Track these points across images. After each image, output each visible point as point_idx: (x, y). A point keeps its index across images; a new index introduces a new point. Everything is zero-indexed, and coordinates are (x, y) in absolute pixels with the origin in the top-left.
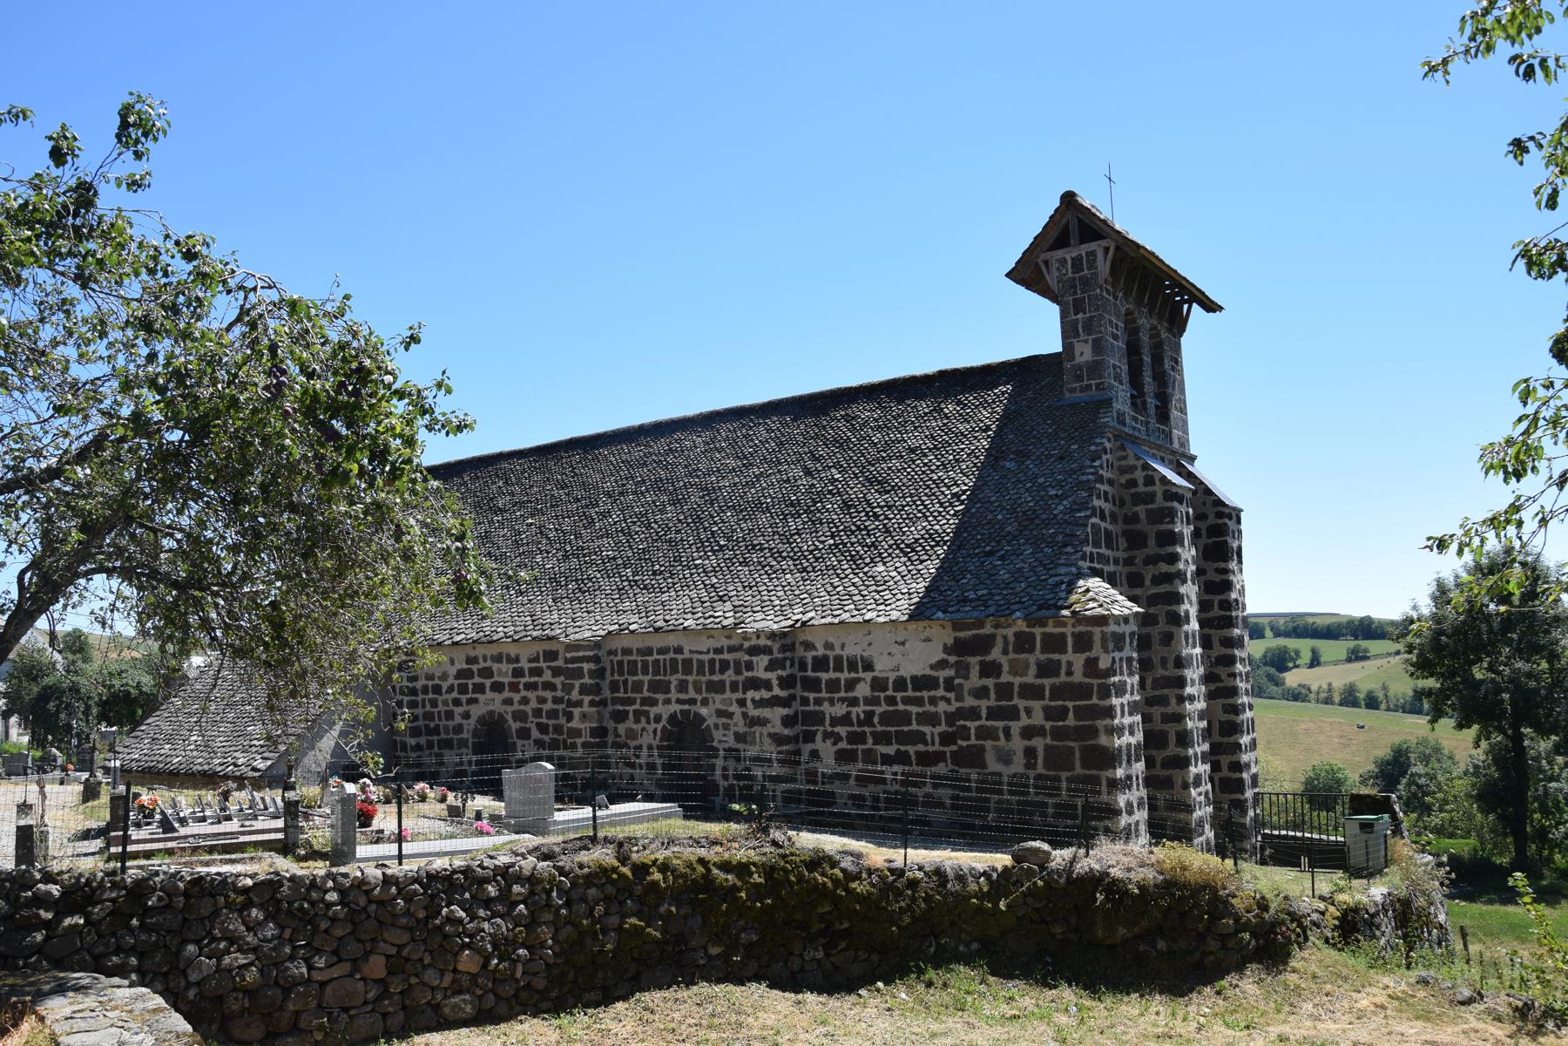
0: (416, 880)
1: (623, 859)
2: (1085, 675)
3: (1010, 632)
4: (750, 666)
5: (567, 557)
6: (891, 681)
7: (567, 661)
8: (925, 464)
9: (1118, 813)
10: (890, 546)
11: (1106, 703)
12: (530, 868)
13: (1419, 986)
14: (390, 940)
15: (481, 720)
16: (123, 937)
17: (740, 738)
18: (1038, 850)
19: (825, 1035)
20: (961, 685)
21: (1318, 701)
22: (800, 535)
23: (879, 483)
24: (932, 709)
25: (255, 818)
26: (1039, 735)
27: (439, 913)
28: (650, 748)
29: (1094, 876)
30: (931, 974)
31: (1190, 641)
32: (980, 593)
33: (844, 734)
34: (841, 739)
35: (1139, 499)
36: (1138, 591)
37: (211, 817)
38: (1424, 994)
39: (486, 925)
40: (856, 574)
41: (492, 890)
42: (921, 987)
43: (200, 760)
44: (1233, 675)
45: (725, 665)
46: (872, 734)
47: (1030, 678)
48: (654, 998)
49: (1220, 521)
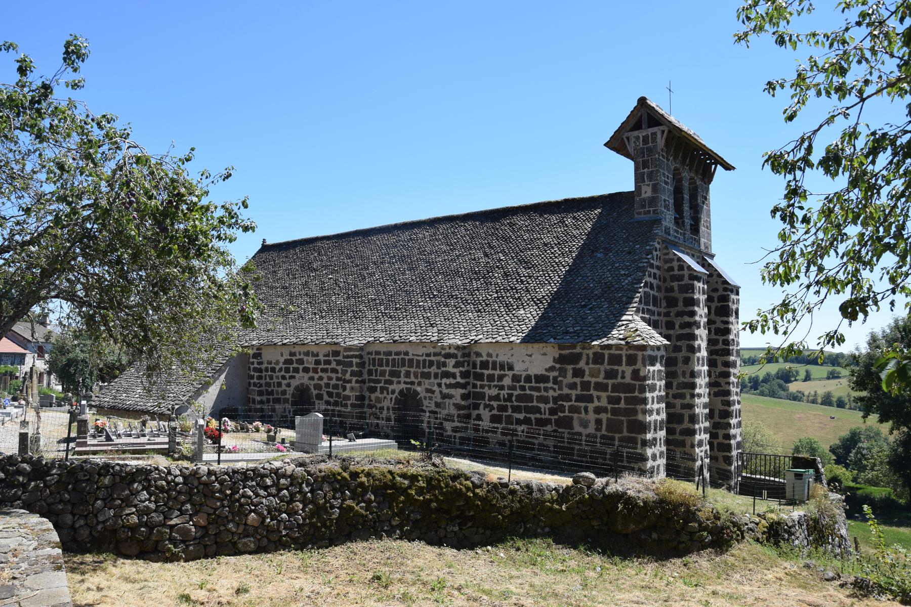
0: (227, 473)
1: (345, 469)
2: (632, 379)
3: (590, 352)
4: (444, 365)
5: (349, 298)
6: (523, 377)
7: (344, 357)
8: (552, 253)
9: (647, 460)
10: (529, 299)
11: (643, 396)
12: (291, 470)
13: (805, 569)
14: (210, 505)
15: (297, 388)
16: (64, 494)
17: (438, 405)
18: (587, 477)
19: (449, 573)
20: (561, 381)
21: (808, 401)
22: (478, 291)
23: (525, 262)
24: (545, 394)
25: (158, 436)
26: (605, 412)
27: (238, 492)
28: (388, 409)
29: (618, 494)
30: (520, 543)
31: (701, 362)
32: (575, 329)
33: (495, 406)
34: (494, 409)
35: (675, 278)
36: (671, 332)
37: (134, 434)
38: (806, 573)
39: (264, 500)
40: (508, 315)
41: (269, 482)
42: (513, 551)
43: (141, 403)
44: (729, 383)
45: (431, 363)
46: (511, 406)
47: (600, 379)
48: (358, 546)
49: (726, 293)
